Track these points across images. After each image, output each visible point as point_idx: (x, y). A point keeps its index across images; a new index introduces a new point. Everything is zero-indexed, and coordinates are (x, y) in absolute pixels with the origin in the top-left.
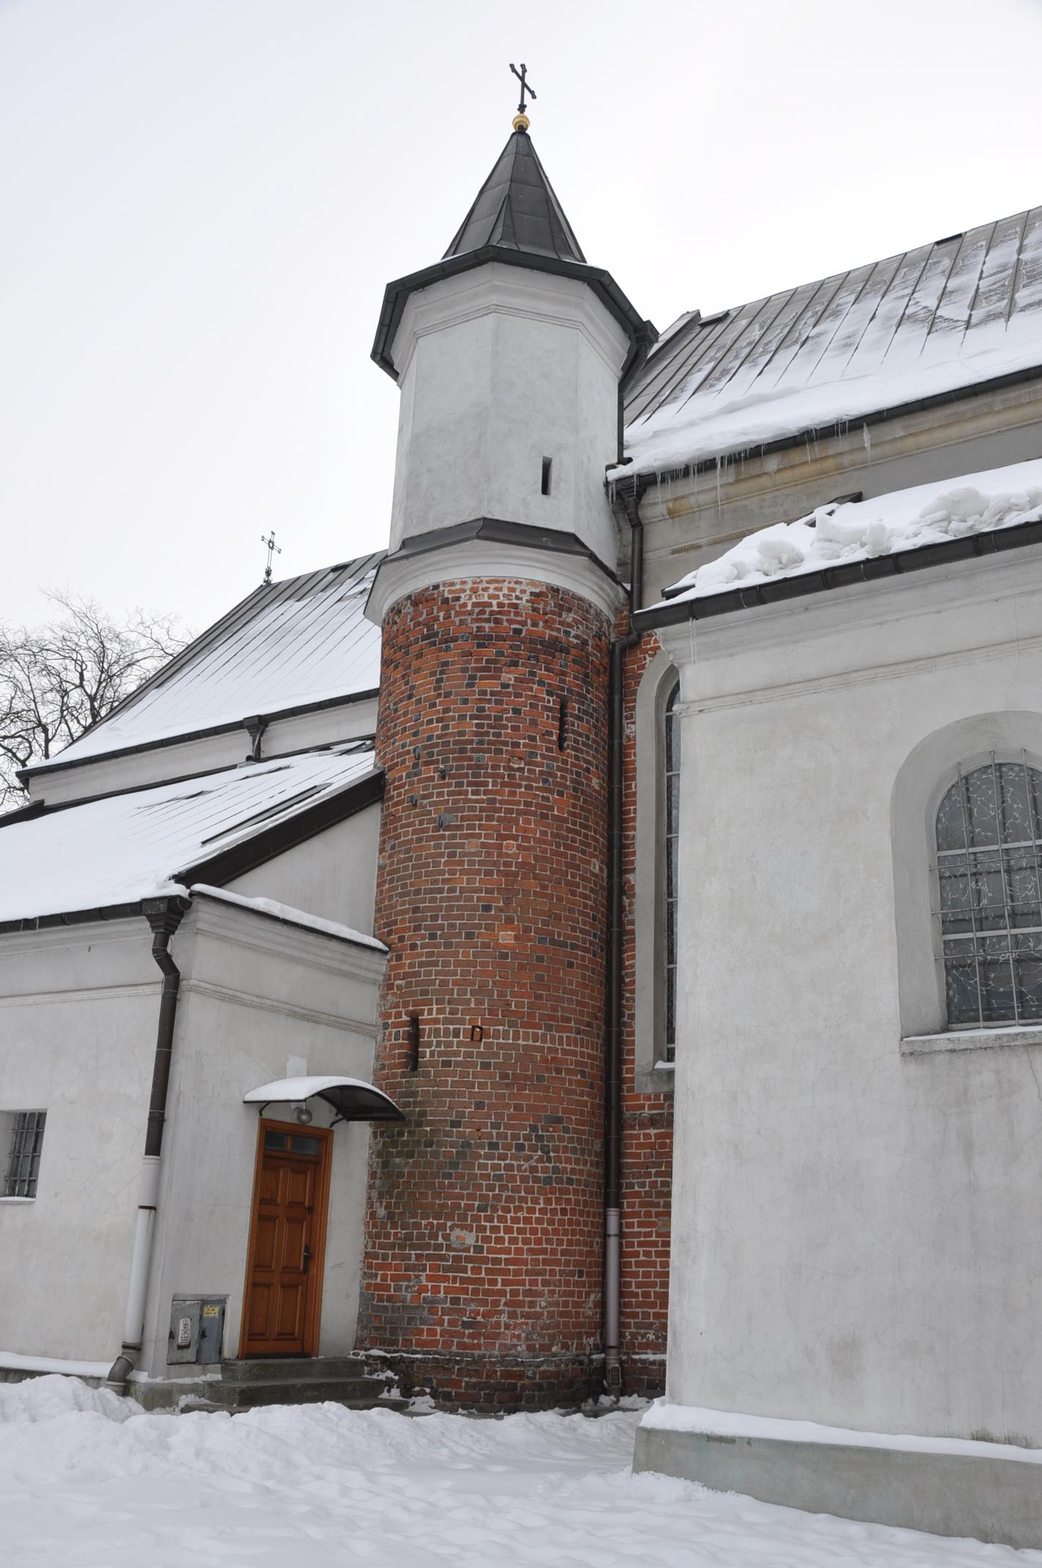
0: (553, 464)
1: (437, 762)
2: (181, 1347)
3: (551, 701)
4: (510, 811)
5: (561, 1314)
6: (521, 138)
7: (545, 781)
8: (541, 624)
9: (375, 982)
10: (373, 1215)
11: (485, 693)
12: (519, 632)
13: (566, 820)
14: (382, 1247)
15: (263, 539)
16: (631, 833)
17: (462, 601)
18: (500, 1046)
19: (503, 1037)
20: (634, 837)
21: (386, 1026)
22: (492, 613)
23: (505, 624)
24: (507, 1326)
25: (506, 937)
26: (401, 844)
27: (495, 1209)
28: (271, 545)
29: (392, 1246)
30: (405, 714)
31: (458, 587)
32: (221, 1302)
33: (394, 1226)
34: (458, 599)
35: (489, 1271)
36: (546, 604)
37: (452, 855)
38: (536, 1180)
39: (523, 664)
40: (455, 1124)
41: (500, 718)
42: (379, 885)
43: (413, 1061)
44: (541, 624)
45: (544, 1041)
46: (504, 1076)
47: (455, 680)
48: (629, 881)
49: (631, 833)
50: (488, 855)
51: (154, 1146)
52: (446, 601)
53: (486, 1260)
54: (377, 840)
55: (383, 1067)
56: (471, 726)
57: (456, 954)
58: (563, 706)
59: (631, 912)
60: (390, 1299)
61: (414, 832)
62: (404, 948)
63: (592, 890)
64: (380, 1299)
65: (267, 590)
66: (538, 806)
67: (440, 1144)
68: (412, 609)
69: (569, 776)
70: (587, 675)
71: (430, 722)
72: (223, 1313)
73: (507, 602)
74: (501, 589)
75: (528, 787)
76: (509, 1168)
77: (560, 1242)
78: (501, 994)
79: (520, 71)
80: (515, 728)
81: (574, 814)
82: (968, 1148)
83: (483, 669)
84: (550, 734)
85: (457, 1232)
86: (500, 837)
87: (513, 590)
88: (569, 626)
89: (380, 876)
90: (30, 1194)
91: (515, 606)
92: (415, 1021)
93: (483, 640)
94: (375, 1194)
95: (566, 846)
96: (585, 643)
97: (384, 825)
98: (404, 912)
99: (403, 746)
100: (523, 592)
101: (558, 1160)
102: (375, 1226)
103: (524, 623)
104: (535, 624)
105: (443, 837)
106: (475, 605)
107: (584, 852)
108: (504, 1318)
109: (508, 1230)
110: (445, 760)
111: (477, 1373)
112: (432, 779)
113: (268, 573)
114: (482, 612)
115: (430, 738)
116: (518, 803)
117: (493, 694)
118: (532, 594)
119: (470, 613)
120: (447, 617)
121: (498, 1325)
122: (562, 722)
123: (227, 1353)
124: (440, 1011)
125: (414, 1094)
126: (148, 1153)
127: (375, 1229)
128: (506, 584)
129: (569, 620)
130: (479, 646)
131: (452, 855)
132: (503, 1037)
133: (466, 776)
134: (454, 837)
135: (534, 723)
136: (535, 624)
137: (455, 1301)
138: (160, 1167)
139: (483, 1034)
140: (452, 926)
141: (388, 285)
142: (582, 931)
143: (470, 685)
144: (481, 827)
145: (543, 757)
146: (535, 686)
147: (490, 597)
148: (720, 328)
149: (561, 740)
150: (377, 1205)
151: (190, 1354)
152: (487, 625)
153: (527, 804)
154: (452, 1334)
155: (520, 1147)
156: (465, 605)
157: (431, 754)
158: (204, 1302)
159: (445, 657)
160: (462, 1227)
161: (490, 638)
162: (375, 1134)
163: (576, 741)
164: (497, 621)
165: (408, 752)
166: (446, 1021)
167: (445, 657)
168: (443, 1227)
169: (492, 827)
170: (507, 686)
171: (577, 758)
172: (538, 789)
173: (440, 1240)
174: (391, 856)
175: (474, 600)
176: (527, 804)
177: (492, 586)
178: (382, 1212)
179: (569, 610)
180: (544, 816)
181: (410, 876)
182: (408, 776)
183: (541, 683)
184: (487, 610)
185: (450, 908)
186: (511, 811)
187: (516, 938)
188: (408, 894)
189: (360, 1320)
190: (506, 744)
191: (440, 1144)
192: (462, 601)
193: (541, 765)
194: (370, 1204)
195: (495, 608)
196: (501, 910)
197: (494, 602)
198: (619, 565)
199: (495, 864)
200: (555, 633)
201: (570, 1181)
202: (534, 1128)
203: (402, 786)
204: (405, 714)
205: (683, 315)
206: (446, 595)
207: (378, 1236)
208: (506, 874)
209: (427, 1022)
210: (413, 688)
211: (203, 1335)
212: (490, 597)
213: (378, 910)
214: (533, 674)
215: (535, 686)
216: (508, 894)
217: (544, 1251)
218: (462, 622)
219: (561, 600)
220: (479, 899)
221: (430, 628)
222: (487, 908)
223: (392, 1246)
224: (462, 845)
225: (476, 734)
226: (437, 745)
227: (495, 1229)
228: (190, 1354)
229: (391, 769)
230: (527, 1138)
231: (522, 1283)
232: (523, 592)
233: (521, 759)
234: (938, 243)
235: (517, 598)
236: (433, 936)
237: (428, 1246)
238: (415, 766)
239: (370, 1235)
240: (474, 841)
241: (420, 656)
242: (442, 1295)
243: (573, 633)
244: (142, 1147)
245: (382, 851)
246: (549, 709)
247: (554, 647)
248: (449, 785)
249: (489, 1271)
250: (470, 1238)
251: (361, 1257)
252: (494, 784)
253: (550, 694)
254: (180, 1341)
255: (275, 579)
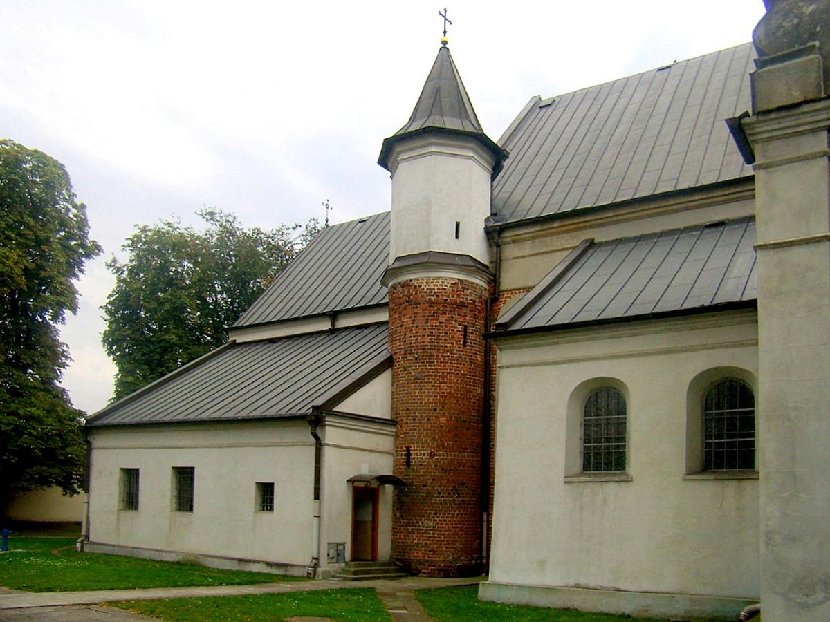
0: (460, 224)
1: (414, 353)
2: (331, 558)
3: (461, 328)
4: (443, 373)
5: (465, 547)
6: (444, 51)
7: (458, 360)
8: (456, 296)
9: (392, 435)
10: (395, 515)
11: (432, 326)
12: (446, 300)
13: (466, 375)
14: (399, 526)
15: (323, 204)
16: (494, 376)
17: (422, 287)
18: (441, 459)
19: (442, 455)
20: (495, 377)
21: (397, 451)
22: (435, 293)
23: (440, 297)
24: (445, 551)
25: (443, 420)
26: (400, 384)
27: (440, 514)
28: (327, 206)
29: (403, 526)
30: (400, 332)
31: (420, 281)
32: (343, 544)
33: (403, 519)
34: (421, 286)
35: (438, 534)
36: (458, 288)
37: (421, 389)
38: (455, 504)
39: (448, 314)
40: (424, 486)
41: (439, 336)
42: (392, 399)
43: (408, 463)
44: (456, 296)
45: (458, 456)
46: (443, 469)
47: (420, 321)
48: (492, 395)
49: (494, 376)
50: (435, 389)
51: (317, 496)
52: (415, 287)
53: (437, 530)
54: (390, 383)
55: (397, 465)
56: (427, 340)
57: (423, 426)
58: (466, 328)
59: (494, 406)
60: (402, 542)
61: (406, 380)
62: (403, 424)
63: (477, 400)
64: (399, 542)
65: (327, 230)
66: (455, 370)
67: (419, 492)
68: (401, 289)
69: (468, 357)
70: (475, 315)
71: (411, 337)
72: (344, 548)
73: (441, 288)
74: (438, 282)
75: (451, 363)
76: (445, 500)
77: (464, 524)
78: (441, 441)
79: (443, 13)
80: (445, 340)
81: (470, 372)
82: (581, 509)
83: (431, 316)
84: (460, 341)
85: (426, 521)
86: (440, 383)
87: (444, 282)
88: (468, 295)
89: (392, 395)
90: (193, 468)
91: (445, 289)
92: (408, 449)
93: (431, 304)
94: (395, 509)
95: (467, 385)
96: (475, 302)
97: (393, 376)
98: (403, 410)
99: (400, 345)
100: (448, 283)
101: (464, 497)
102: (396, 519)
103: (448, 296)
104: (453, 296)
105: (417, 382)
106: (427, 289)
107: (474, 386)
108: (444, 549)
109: (445, 521)
110: (417, 353)
111: (435, 566)
112: (412, 360)
113: (327, 221)
114: (431, 292)
115: (411, 343)
116: (447, 369)
117: (436, 326)
118: (452, 284)
119: (426, 293)
120: (416, 294)
121: (442, 551)
122: (465, 335)
123: (346, 560)
124: (417, 447)
125: (409, 475)
126: (315, 499)
127: (396, 520)
128: (440, 281)
129: (468, 293)
130: (430, 306)
131: (421, 389)
132: (442, 455)
133: (426, 359)
134: (422, 383)
135: (453, 337)
136: (453, 296)
137: (426, 543)
138: (320, 503)
139: (435, 455)
140: (421, 416)
141: (385, 140)
142: (474, 416)
143: (426, 323)
144: (432, 379)
145: (457, 351)
146: (453, 322)
147: (434, 285)
148: (550, 109)
149: (465, 342)
150: (396, 512)
151: (334, 560)
152: (433, 298)
153: (450, 370)
154: (425, 554)
155: (449, 494)
156: (423, 289)
157: (411, 350)
158: (338, 544)
159: (415, 311)
160: (428, 520)
161: (434, 303)
162: (394, 489)
163: (471, 343)
164: (437, 296)
165: (402, 349)
166: (420, 450)
167: (415, 311)
168: (421, 520)
169: (436, 379)
170: (442, 323)
171: (471, 350)
172: (455, 363)
173: (420, 524)
174: (397, 388)
175: (427, 287)
176: (450, 370)
177: (435, 281)
178: (398, 515)
179: (468, 289)
180: (458, 374)
181: (404, 397)
182: (402, 358)
183: (456, 321)
184: (433, 291)
185: (420, 410)
186: (444, 373)
187: (447, 420)
188: (404, 403)
189: (392, 549)
190: (442, 346)
191: (419, 492)
192: (422, 287)
193: (456, 354)
194: (394, 512)
195: (436, 291)
196: (441, 410)
197: (436, 288)
198: (491, 262)
199: (438, 393)
200: (462, 300)
201: (468, 504)
202: (454, 487)
203: (400, 361)
204: (400, 332)
205: (532, 98)
206: (415, 284)
207: (397, 522)
208: (442, 397)
209: (412, 450)
210: (403, 322)
211: (338, 555)
212: (434, 285)
213: (392, 408)
214: (452, 317)
215: (453, 322)
216: (443, 404)
217: (458, 527)
218: (422, 296)
219: (465, 285)
220: (432, 406)
221: (409, 298)
222: (435, 410)
223: (403, 526)
224: (425, 386)
225: (430, 342)
226: (413, 346)
227: (440, 521)
228: (334, 560)
229: (395, 354)
230: (452, 490)
231: (450, 538)
232: (448, 283)
233: (448, 352)
234: (659, 70)
235: (446, 286)
236: (414, 420)
237: (415, 526)
238: (405, 354)
239: (393, 522)
240: (430, 385)
241: (405, 309)
242: (421, 541)
243: (469, 298)
244: (313, 497)
245: (393, 385)
246: (459, 331)
247: (462, 305)
248: (419, 363)
249: (438, 534)
250: (431, 524)
251: (391, 529)
252: (437, 362)
253: (459, 325)
254: (331, 556)
255: (330, 224)
